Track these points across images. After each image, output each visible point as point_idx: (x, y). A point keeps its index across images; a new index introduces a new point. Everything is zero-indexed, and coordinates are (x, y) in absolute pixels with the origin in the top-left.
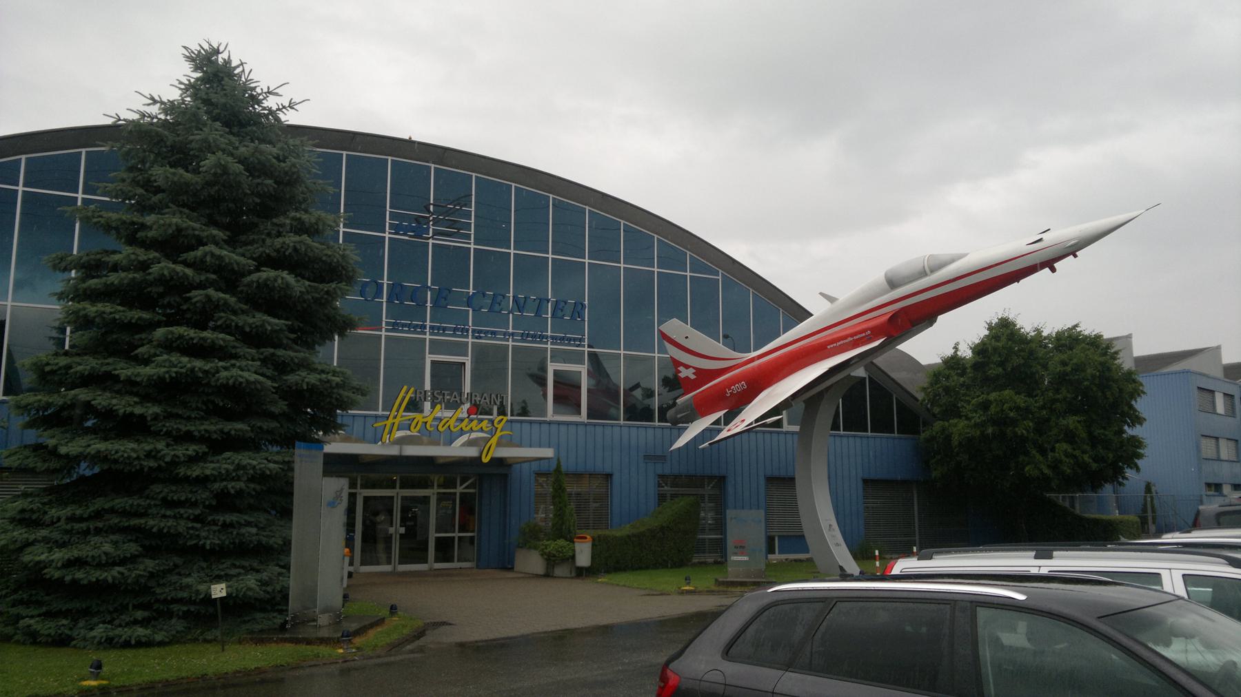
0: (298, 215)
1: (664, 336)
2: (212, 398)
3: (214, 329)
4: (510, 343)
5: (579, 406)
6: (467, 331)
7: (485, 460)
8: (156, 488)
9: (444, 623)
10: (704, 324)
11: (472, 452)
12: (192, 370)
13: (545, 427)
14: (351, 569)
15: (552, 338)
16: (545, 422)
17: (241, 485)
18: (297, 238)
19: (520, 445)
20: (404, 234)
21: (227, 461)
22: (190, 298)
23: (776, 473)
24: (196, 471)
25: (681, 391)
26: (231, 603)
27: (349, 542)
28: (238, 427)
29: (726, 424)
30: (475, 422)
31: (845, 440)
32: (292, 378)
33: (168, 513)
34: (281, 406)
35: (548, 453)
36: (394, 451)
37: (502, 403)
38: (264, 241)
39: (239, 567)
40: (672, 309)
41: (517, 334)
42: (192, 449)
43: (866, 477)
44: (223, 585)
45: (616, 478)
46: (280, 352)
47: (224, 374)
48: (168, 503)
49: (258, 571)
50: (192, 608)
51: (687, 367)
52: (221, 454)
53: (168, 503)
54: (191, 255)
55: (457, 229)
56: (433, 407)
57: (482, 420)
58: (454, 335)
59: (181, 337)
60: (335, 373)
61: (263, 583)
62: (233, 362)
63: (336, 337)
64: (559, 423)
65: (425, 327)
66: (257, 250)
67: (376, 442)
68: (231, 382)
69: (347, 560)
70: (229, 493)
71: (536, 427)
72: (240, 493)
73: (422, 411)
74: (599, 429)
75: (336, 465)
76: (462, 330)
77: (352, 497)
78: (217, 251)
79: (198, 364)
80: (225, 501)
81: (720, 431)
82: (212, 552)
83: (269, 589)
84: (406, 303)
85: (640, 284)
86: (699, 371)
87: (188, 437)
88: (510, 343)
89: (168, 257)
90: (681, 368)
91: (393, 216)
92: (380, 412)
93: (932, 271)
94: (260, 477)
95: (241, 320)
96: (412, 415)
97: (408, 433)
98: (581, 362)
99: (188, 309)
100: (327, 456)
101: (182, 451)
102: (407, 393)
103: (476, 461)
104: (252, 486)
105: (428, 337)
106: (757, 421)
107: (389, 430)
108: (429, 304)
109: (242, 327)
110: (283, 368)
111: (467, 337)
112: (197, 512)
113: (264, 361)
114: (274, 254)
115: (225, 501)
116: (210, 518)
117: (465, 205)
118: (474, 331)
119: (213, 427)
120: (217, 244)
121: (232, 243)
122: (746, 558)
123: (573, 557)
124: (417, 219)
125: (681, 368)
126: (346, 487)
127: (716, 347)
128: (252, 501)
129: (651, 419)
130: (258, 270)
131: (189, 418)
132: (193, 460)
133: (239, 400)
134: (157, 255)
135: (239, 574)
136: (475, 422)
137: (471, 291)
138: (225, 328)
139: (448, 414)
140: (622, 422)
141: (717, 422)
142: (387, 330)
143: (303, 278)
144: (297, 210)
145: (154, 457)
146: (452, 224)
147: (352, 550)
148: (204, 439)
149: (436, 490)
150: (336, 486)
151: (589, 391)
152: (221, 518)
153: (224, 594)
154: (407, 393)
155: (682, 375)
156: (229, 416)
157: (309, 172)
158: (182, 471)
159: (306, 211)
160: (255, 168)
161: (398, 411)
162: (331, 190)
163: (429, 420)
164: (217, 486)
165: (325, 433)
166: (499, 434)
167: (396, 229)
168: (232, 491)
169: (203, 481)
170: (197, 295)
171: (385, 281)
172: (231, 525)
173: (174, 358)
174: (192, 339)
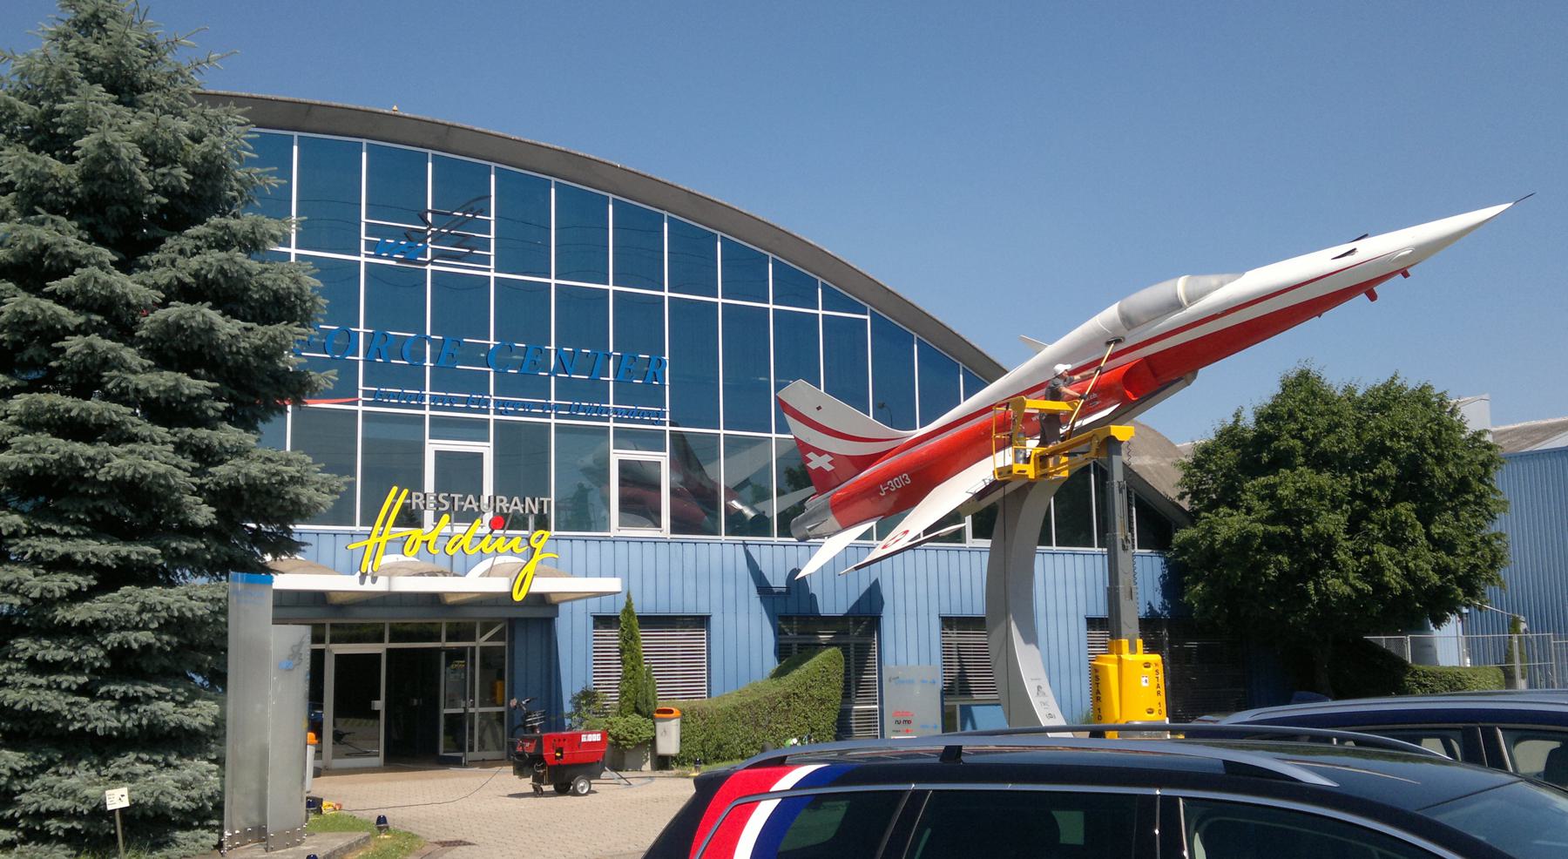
0: (223, 221)
1: (782, 406)
2: (101, 503)
3: (107, 396)
4: (553, 421)
5: (659, 514)
6: (487, 402)
7: (518, 597)
8: (22, 643)
9: (466, 844)
10: (847, 389)
11: (499, 585)
12: (71, 457)
13: (607, 546)
14: (320, 764)
15: (616, 411)
16: (607, 539)
17: (146, 637)
18: (223, 255)
19: (572, 574)
20: (390, 258)
21: (124, 601)
22: (63, 350)
23: (956, 612)
24: (81, 613)
25: (812, 489)
26: (138, 813)
27: (316, 726)
28: (136, 551)
29: (881, 537)
30: (502, 539)
31: (1059, 558)
32: (221, 470)
33: (43, 681)
34: (204, 515)
35: (613, 584)
36: (381, 586)
37: (541, 510)
38: (173, 262)
39: (147, 762)
40: (797, 365)
42: (73, 581)
43: (946, 612)
44: (124, 790)
45: (715, 623)
46: (203, 433)
47: (117, 462)
48: (36, 666)
49: (176, 767)
50: (77, 825)
51: (820, 452)
52: (116, 589)
53: (36, 666)
54: (54, 285)
55: (470, 249)
56: (437, 518)
57: (511, 538)
59: (52, 408)
60: (288, 462)
61: (185, 786)
62: (130, 446)
63: (289, 408)
64: (628, 541)
65: (423, 398)
66: (163, 276)
67: (352, 573)
68: (129, 473)
69: (311, 750)
70: (130, 647)
71: (593, 546)
72: (146, 648)
73: (419, 525)
74: (689, 548)
75: (292, 606)
76: (478, 401)
77: (317, 658)
78: (103, 276)
79: (80, 448)
80: (126, 664)
81: (870, 548)
82: (108, 738)
83: (195, 793)
84: (395, 373)
85: (746, 325)
86: (837, 459)
87: (65, 564)
88: (553, 421)
89: (26, 288)
90: (811, 455)
91: (371, 229)
92: (358, 528)
93: (1191, 301)
94: (177, 624)
95: (141, 381)
96: (405, 531)
97: (401, 558)
99: (61, 367)
100: (276, 591)
101: (60, 583)
102: (397, 497)
103: (504, 599)
104: (165, 638)
106: (926, 532)
107: (615, 632)
108: (428, 363)
109: (146, 391)
110: (206, 456)
112: (82, 679)
113: (180, 448)
114: (189, 280)
115: (126, 664)
116: (103, 689)
117: (481, 213)
118: (433, 398)
119: (104, 550)
120: (101, 266)
121: (125, 266)
123: (653, 741)
124: (408, 235)
125: (811, 455)
126: (308, 639)
127: (866, 423)
128: (166, 662)
129: (768, 533)
130: (164, 304)
131: (66, 537)
132: (76, 596)
133: (138, 508)
134: (11, 285)
135: (147, 773)
136: (502, 539)
138: (121, 397)
139: (460, 528)
141: (866, 535)
142: (365, 404)
143: (235, 316)
144: (223, 215)
145: (15, 592)
146: (462, 241)
147: (319, 735)
148: (98, 569)
150: (298, 635)
151: (673, 492)
152: (120, 689)
153: (125, 803)
154: (397, 497)
155: (813, 465)
156: (128, 536)
157: (239, 158)
158: (62, 614)
159: (235, 216)
160: (158, 153)
161: (384, 525)
162: (274, 182)
163: (433, 538)
164: (113, 639)
165: (275, 556)
166: (537, 557)
168: (135, 646)
169: (88, 631)
170: (74, 344)
171: (361, 329)
172: (136, 700)
173: (44, 439)
174: (69, 410)
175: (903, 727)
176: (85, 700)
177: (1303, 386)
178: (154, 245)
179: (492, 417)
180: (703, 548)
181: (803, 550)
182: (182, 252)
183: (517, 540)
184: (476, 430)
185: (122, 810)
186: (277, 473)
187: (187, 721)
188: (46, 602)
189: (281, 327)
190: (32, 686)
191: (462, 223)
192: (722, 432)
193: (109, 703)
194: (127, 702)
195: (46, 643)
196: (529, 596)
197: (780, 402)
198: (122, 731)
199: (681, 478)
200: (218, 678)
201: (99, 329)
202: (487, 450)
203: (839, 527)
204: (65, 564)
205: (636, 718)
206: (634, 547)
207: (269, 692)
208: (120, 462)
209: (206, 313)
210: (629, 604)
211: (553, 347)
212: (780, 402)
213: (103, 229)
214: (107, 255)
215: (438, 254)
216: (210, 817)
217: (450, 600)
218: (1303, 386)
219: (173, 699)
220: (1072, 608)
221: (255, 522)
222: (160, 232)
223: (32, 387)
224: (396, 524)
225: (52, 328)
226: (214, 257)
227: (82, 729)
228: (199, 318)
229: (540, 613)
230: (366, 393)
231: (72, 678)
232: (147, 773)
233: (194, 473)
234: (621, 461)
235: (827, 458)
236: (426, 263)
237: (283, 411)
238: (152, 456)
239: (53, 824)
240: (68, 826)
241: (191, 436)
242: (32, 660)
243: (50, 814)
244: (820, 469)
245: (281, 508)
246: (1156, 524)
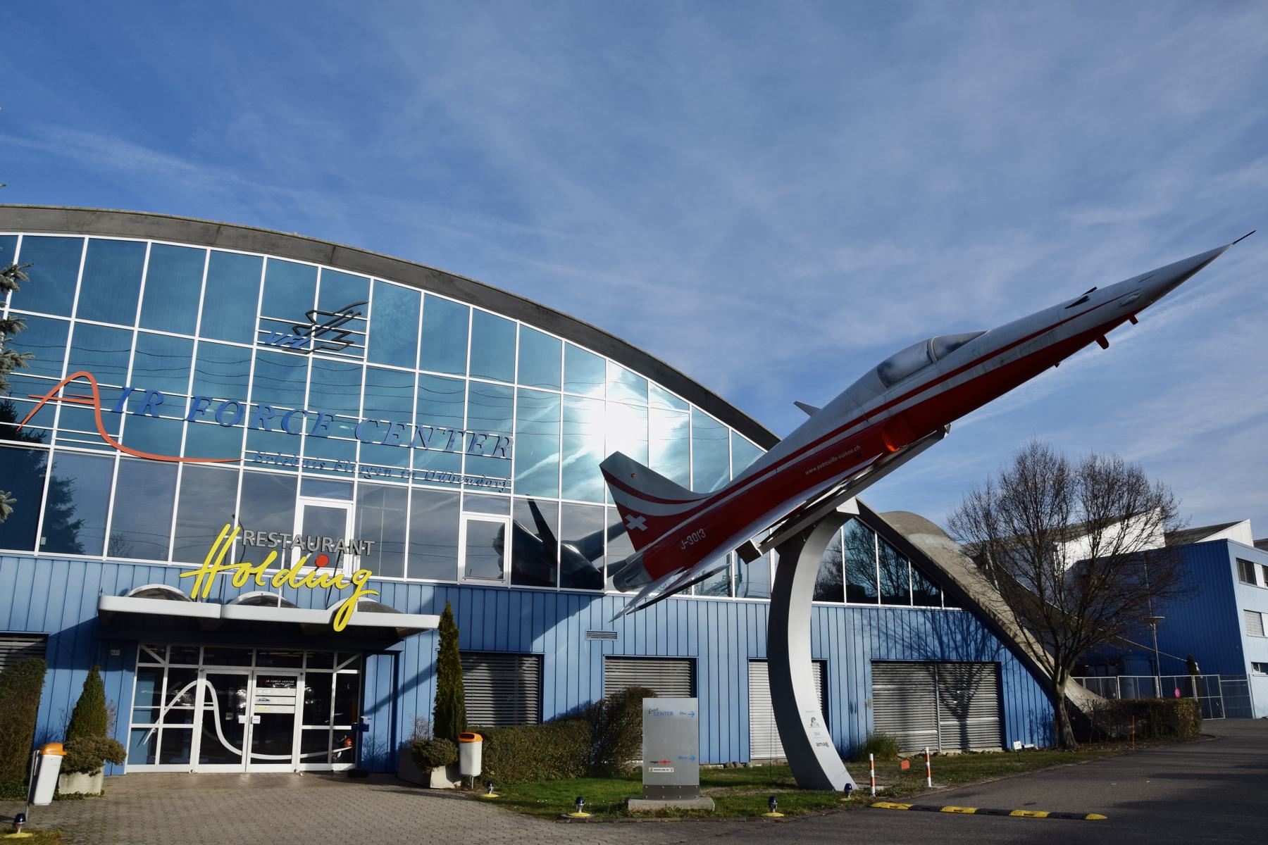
4: (410, 485)
6: (353, 467)
7: (338, 628)
16: (402, 583)
41: (420, 474)
43: (876, 657)
51: (636, 515)
58: (335, 472)
65: (297, 461)
76: (346, 466)
86: (650, 520)
88: (410, 485)
98: (507, 511)
105: (300, 474)
111: (352, 475)
118: (362, 468)
122: (349, 728)
124: (296, 329)
140: (558, 589)
142: (246, 464)
149: (305, 670)
161: (212, 562)
167: (266, 340)
171: (249, 403)
179: (356, 479)
180: (539, 597)
184: (344, 490)
196: (348, 627)
211: (414, 424)
215: (320, 346)
220: (859, 653)
234: (306, 507)
235: (642, 519)
236: (308, 352)
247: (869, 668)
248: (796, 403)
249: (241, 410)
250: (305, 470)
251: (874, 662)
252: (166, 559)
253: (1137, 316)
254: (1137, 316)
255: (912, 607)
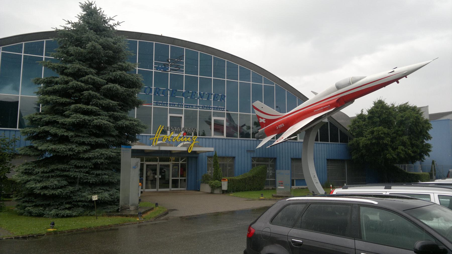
1: (254, 107)
4: (198, 110)
7: (189, 152)
8: (73, 161)
10: (269, 103)
11: (185, 149)
13: (211, 140)
15: (213, 108)
16: (211, 138)
17: (102, 160)
19: (202, 147)
20: (160, 70)
21: (97, 152)
22: (83, 94)
23: (295, 157)
24: (86, 156)
26: (99, 202)
29: (277, 139)
32: (120, 123)
33: (77, 170)
34: (116, 133)
35: (212, 149)
36: (157, 148)
38: (109, 73)
40: (257, 97)
41: (201, 106)
42: (85, 148)
43: (292, 157)
44: (96, 196)
45: (236, 159)
46: (115, 113)
47: (96, 121)
49: (109, 191)
51: (262, 118)
54: (81, 79)
56: (171, 133)
57: (188, 137)
58: (178, 107)
59: (80, 108)
60: (135, 121)
61: (111, 195)
62: (99, 117)
64: (216, 139)
66: (107, 76)
69: (140, 187)
72: (102, 163)
75: (136, 153)
77: (142, 165)
78: (93, 77)
79: (86, 117)
80: (97, 166)
81: (274, 141)
82: (93, 184)
83: (113, 197)
85: (245, 88)
86: (266, 120)
87: (83, 144)
88: (198, 110)
90: (260, 119)
91: (155, 63)
94: (109, 158)
95: (101, 102)
96: (163, 135)
97: (162, 142)
102: (161, 127)
103: (186, 152)
106: (288, 138)
108: (169, 96)
109: (102, 104)
110: (116, 119)
112: (87, 170)
113: (110, 116)
115: (97, 166)
116: (91, 172)
117: (182, 59)
118: (185, 105)
119: (93, 140)
120: (92, 74)
121: (98, 74)
123: (221, 187)
124: (164, 65)
125: (260, 119)
128: (106, 166)
130: (107, 84)
132: (85, 152)
133: (101, 131)
135: (102, 192)
137: (184, 91)
138: (96, 105)
139: (176, 135)
140: (239, 138)
141: (273, 138)
142: (154, 105)
143: (123, 86)
145: (72, 151)
147: (142, 183)
150: (138, 160)
154: (161, 127)
155: (260, 121)
156: (97, 136)
158: (81, 156)
159: (124, 62)
160: (105, 47)
164: (94, 161)
165: (132, 142)
166: (194, 142)
168: (99, 163)
169: (89, 159)
170: (86, 93)
172: (99, 175)
173: (78, 115)
174: (84, 109)
175: (281, 185)
176: (87, 175)
177: (380, 105)
178: (104, 68)
179: (184, 109)
180: (234, 141)
181: (258, 142)
182: (111, 71)
183: (189, 139)
185: (96, 200)
186: (133, 124)
187: (111, 180)
188: (79, 153)
189: (134, 89)
190: (76, 171)
191: (177, 62)
192: (239, 113)
193: (94, 176)
194: (97, 175)
195: (79, 162)
196: (192, 151)
197: (252, 105)
198: (96, 182)
199: (228, 124)
200: (118, 170)
201: (91, 89)
202: (183, 116)
203: (362, 209)
204: (83, 144)
205: (217, 181)
206: (217, 140)
207: (130, 183)
208: (97, 121)
209: (117, 86)
210: (216, 154)
212: (252, 105)
213: (92, 65)
214: (93, 71)
215: (171, 70)
216: (116, 202)
217: (173, 152)
218: (380, 105)
219: (108, 175)
221: (129, 133)
222: (106, 65)
223: (76, 102)
224: (161, 134)
225: (80, 89)
226: (119, 72)
227: (87, 182)
228: (115, 88)
229: (194, 155)
230: (154, 103)
231: (85, 170)
232: (102, 192)
233: (113, 123)
234: (214, 120)
237: (134, 108)
238: (103, 120)
239: (80, 203)
240: (83, 204)
241: (113, 114)
242: (75, 165)
243: (79, 201)
244: (262, 122)
245: (134, 131)
246: (345, 138)
247: (326, 161)
248: (312, 91)
249: (151, 89)
250: (185, 107)
251: (328, 160)
252: (16, 128)
253: (399, 81)
254: (399, 81)
255: (329, 142)
